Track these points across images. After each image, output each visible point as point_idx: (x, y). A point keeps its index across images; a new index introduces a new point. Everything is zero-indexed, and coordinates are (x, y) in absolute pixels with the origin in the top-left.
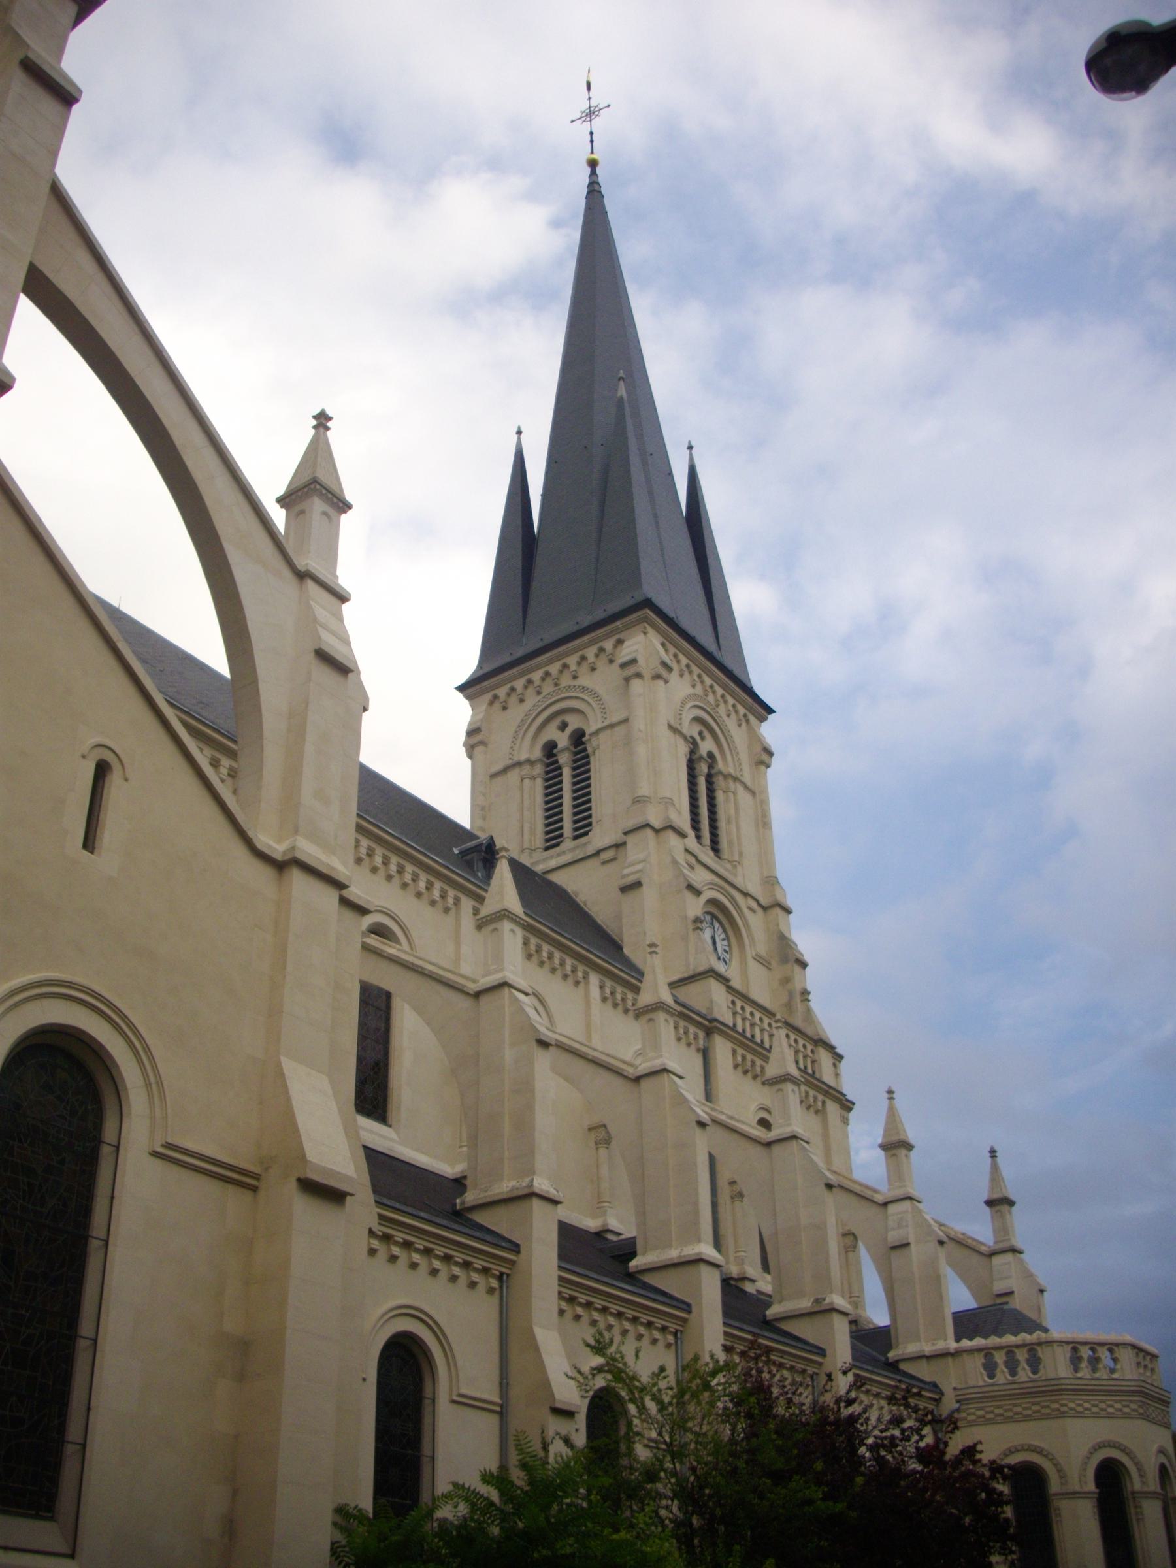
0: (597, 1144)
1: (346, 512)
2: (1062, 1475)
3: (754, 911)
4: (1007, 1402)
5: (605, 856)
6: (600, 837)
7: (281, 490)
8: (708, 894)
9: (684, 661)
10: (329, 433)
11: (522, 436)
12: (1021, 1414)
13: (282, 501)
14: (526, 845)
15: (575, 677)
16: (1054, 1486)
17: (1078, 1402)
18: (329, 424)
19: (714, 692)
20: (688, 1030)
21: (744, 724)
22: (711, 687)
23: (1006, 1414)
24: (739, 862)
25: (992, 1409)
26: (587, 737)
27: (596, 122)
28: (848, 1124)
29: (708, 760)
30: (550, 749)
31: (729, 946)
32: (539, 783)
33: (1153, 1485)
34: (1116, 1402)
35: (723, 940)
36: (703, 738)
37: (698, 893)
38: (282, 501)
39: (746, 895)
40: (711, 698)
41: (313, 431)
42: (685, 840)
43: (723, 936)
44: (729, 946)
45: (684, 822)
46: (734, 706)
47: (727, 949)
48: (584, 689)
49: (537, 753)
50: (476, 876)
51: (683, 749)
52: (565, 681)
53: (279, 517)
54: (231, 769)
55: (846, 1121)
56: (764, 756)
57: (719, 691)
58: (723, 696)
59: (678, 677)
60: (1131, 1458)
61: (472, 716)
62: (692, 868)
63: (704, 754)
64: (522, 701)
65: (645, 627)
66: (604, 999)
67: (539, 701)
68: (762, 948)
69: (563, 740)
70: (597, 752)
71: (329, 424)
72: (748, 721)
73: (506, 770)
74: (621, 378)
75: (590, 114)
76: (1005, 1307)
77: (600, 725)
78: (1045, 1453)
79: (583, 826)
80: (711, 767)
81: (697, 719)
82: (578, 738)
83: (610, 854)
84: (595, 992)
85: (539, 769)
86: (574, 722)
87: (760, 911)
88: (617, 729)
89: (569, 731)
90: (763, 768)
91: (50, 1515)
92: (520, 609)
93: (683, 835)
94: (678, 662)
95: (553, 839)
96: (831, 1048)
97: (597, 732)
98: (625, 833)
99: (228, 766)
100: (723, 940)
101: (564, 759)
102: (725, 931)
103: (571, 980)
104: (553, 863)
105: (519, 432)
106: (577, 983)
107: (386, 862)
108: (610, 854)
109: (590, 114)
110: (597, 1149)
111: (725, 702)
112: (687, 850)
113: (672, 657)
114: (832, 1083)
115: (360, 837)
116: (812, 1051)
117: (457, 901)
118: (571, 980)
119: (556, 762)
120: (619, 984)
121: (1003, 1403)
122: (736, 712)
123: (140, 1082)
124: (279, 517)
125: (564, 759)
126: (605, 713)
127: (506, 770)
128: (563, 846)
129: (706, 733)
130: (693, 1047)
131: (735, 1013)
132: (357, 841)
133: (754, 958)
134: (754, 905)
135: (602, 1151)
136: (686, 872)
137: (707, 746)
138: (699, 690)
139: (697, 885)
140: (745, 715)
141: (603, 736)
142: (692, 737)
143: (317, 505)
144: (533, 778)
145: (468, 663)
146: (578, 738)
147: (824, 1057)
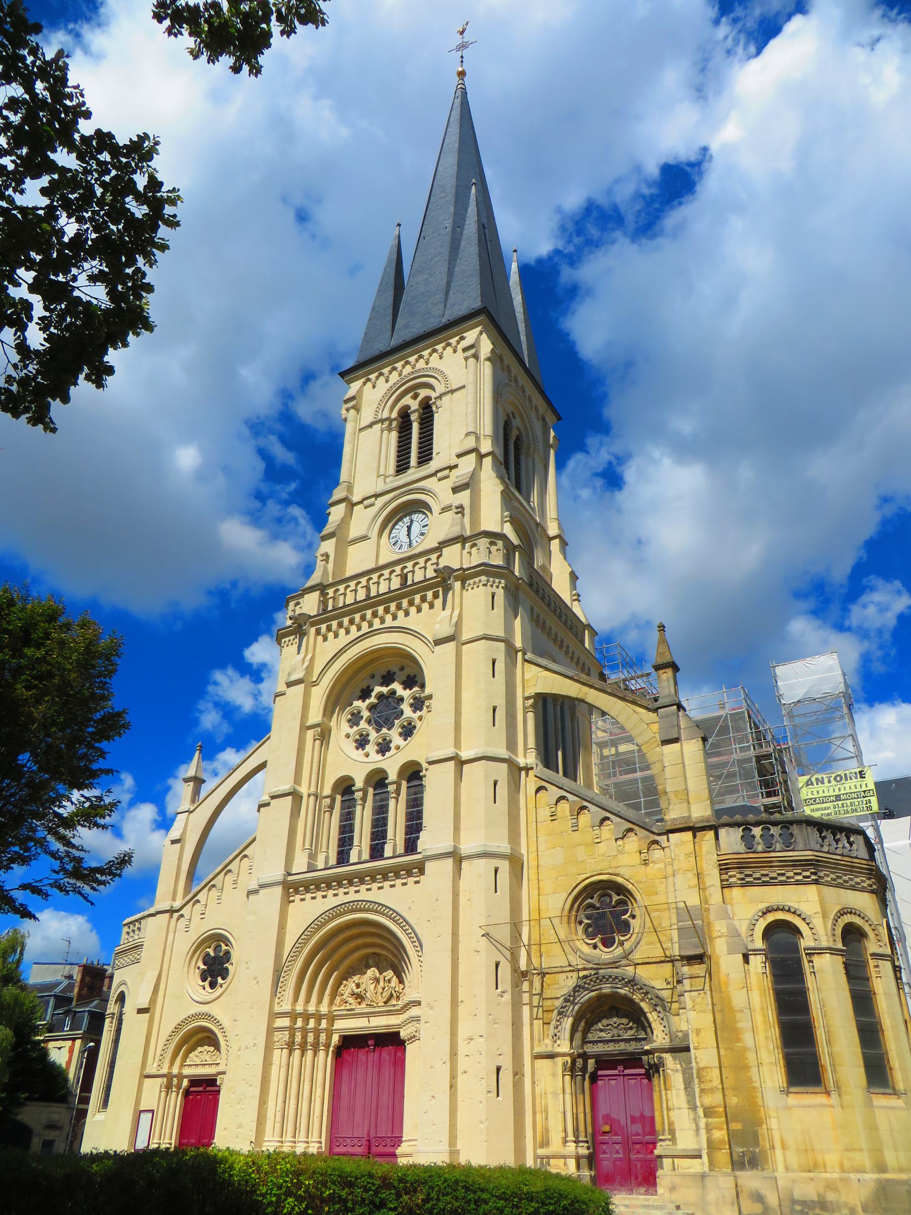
5: (440, 475)
14: (382, 471)
26: (433, 400)
27: (466, 52)
30: (405, 415)
60: (787, 911)
69: (414, 405)
73: (371, 425)
74: (474, 183)
75: (463, 46)
78: (798, 913)
79: (426, 456)
86: (423, 393)
88: (455, 394)
89: (419, 398)
91: (764, 796)
92: (390, 311)
98: (459, 456)
109: (463, 46)
123: (570, 1092)
127: (371, 425)
128: (410, 471)
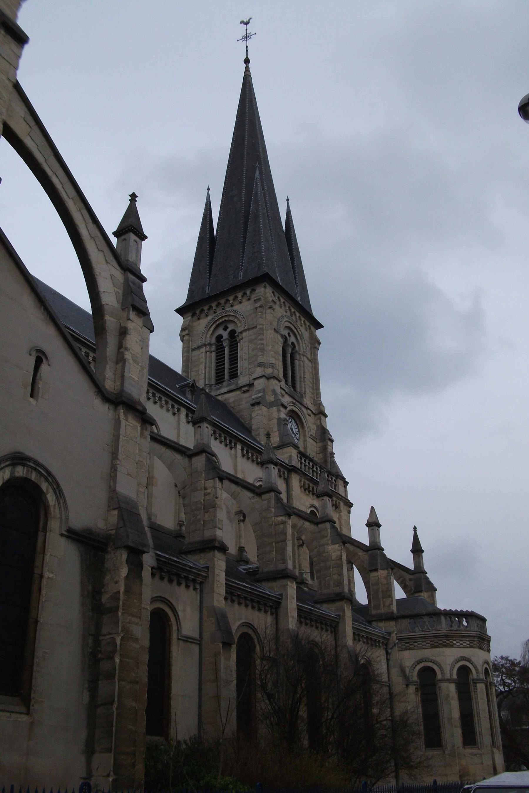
0: (240, 521)
1: (144, 240)
2: (443, 673)
3: (310, 416)
4: (436, 639)
6: (242, 380)
7: (115, 229)
8: (289, 408)
9: (282, 300)
10: (136, 203)
11: (210, 191)
12: (438, 642)
13: (115, 234)
15: (232, 306)
16: (439, 676)
17: (451, 641)
18: (137, 199)
19: (295, 315)
20: (280, 471)
21: (308, 330)
22: (294, 312)
23: (419, 646)
24: (304, 393)
25: (413, 643)
28: (350, 513)
29: (292, 346)
31: (299, 432)
32: (214, 354)
33: (482, 676)
34: (467, 641)
35: (296, 429)
36: (290, 336)
37: (286, 408)
38: (115, 234)
39: (307, 408)
40: (294, 317)
41: (129, 202)
42: (281, 383)
43: (296, 427)
44: (299, 430)
45: (281, 376)
46: (304, 321)
47: (298, 433)
48: (236, 312)
49: (213, 341)
50: (186, 398)
51: (281, 340)
52: (228, 308)
53: (114, 240)
54: (94, 357)
55: (349, 512)
56: (316, 343)
57: (298, 314)
58: (284, 302)
59: (279, 308)
61: (184, 322)
62: (283, 396)
63: (290, 343)
64: (207, 316)
65: (265, 284)
66: (243, 456)
67: (215, 316)
68: (313, 432)
70: (241, 341)
71: (137, 199)
72: (310, 328)
76: (419, 598)
77: (242, 329)
79: (234, 375)
80: (293, 349)
81: (288, 327)
82: (232, 334)
83: (246, 388)
84: (239, 452)
85: (213, 348)
86: (231, 327)
87: (312, 415)
89: (228, 330)
90: (316, 350)
93: (280, 381)
94: (280, 300)
95: (219, 379)
96: (343, 479)
97: (241, 333)
99: (84, 351)
100: (296, 429)
101: (226, 344)
102: (297, 424)
103: (228, 447)
104: (218, 392)
105: (208, 189)
106: (231, 448)
107: (160, 399)
108: (246, 388)
110: (239, 523)
111: (300, 319)
112: (281, 388)
113: (277, 299)
114: (343, 495)
115: (149, 389)
116: (335, 480)
117: (179, 410)
118: (228, 447)
119: (222, 344)
120: (282, 467)
121: (417, 640)
122: (305, 324)
124: (114, 240)
125: (226, 344)
126: (246, 323)
128: (224, 384)
129: (291, 334)
130: (282, 477)
131: (301, 463)
132: (148, 390)
133: (309, 437)
134: (310, 413)
135: (242, 524)
136: (280, 398)
137: (292, 339)
138: (288, 314)
139: (286, 404)
140: (294, 312)
141: (244, 334)
142: (285, 336)
143: (132, 237)
144: (211, 352)
145: (181, 300)
146: (232, 334)
147: (340, 483)
